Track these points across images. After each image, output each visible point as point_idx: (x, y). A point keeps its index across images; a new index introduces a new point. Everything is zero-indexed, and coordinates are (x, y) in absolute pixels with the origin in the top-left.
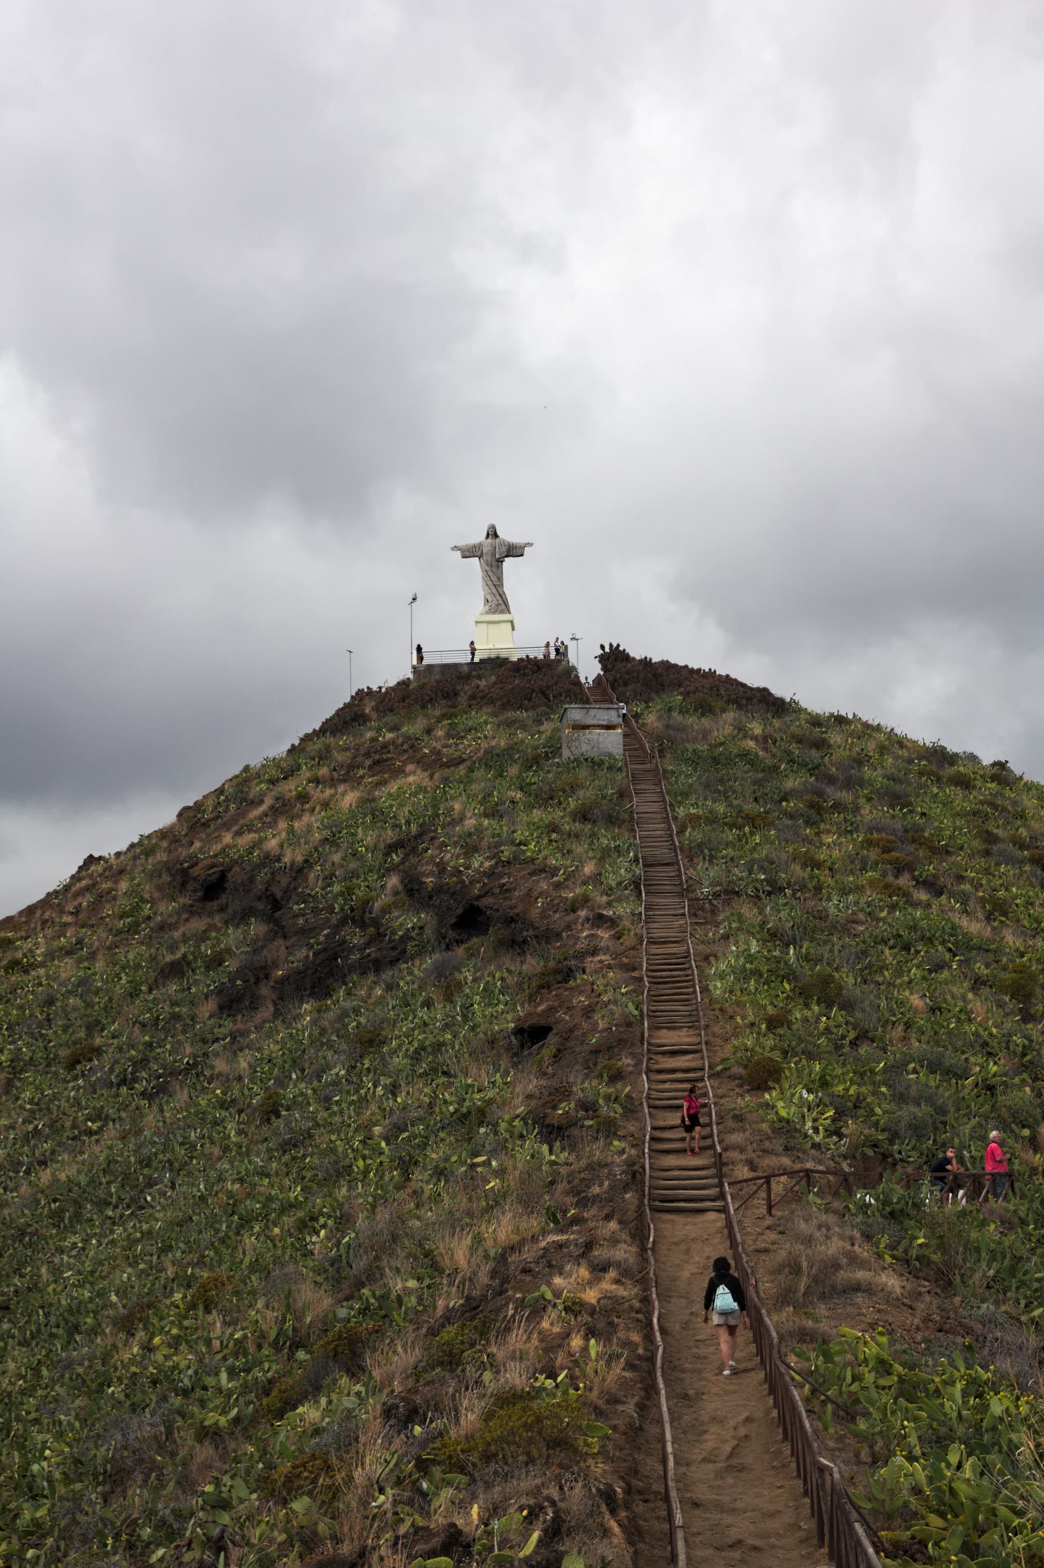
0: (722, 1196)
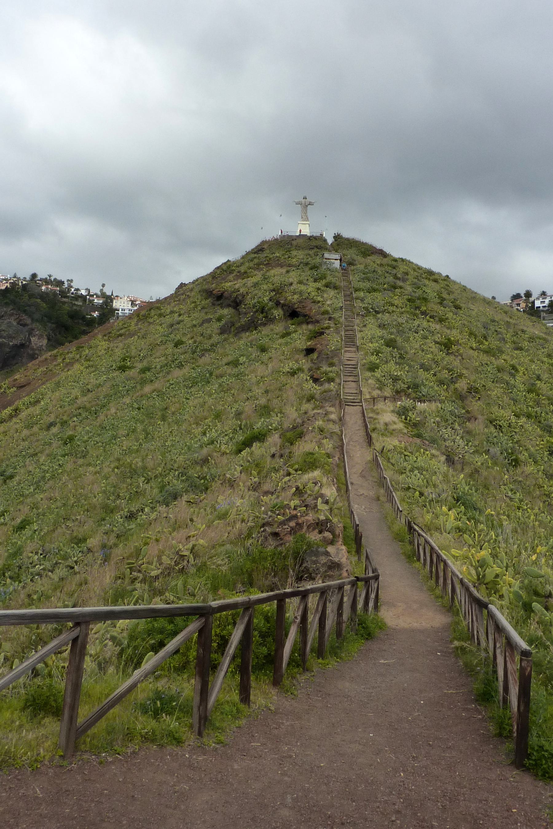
0: (361, 402)
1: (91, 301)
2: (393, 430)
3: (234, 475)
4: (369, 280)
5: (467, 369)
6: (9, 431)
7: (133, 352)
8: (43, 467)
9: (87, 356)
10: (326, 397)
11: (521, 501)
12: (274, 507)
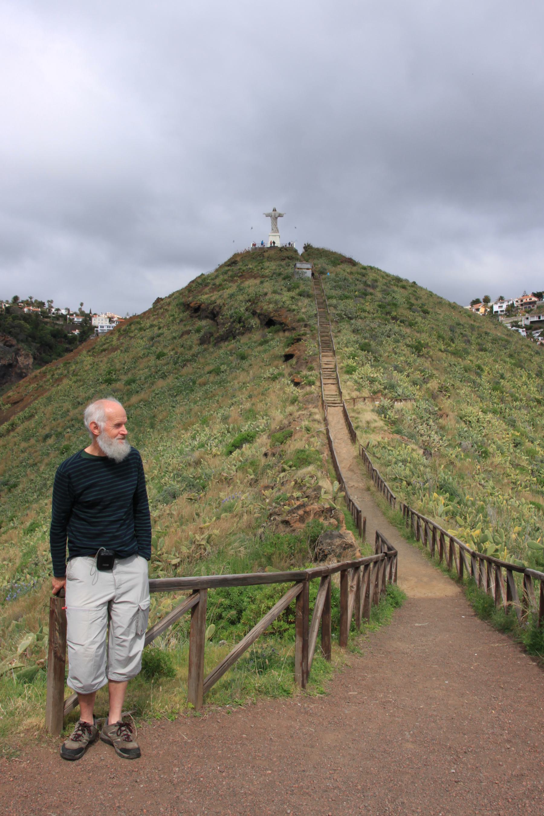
1: (71, 320)
2: (375, 428)
3: (230, 474)
4: (340, 288)
5: (437, 369)
6: (8, 444)
7: (118, 366)
8: (44, 475)
9: (74, 372)
10: (309, 400)
11: (493, 488)
12: (278, 499)
